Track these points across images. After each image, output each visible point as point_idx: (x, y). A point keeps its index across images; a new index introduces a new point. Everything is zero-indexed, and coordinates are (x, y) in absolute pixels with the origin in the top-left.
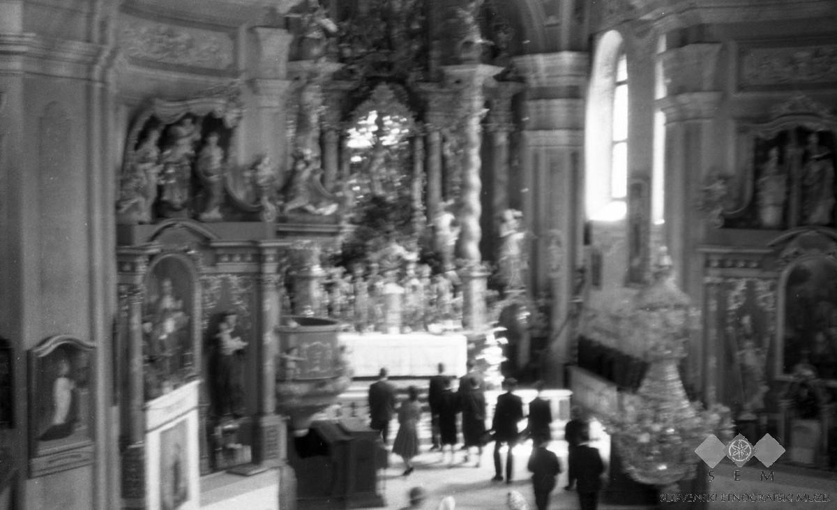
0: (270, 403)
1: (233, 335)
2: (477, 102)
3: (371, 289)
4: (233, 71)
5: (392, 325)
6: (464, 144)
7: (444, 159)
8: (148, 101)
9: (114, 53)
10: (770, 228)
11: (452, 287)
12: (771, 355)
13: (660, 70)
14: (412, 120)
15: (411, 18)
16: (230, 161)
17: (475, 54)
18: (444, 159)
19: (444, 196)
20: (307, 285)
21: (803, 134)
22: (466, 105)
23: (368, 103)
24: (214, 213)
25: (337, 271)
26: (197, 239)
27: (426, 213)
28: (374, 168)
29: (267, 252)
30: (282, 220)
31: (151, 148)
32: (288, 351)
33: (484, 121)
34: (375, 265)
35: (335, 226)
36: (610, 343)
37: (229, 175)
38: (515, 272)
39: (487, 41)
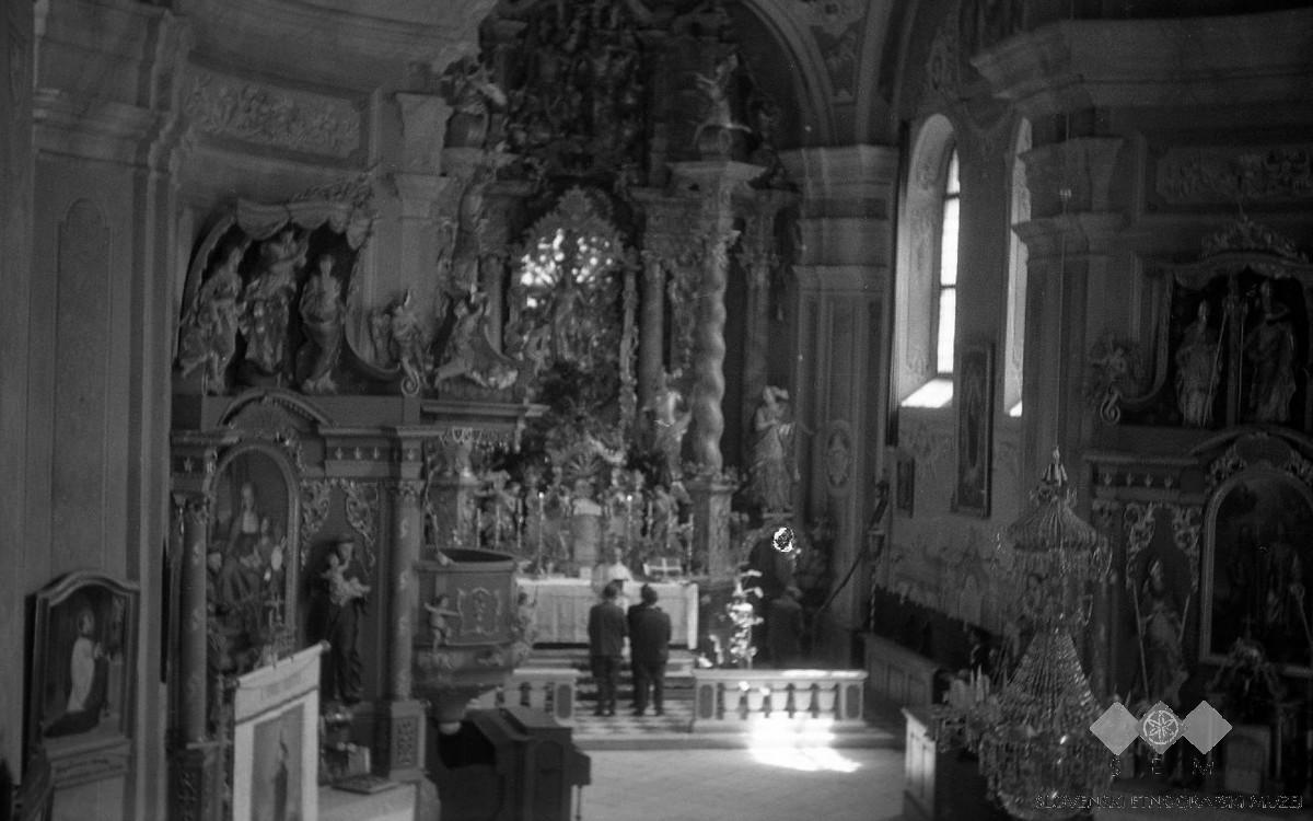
0: (404, 681)
1: (347, 576)
2: (725, 220)
3: (553, 505)
4: (359, 160)
5: (584, 563)
6: (703, 282)
7: (668, 306)
8: (228, 203)
9: (181, 126)
10: (1194, 426)
11: (676, 508)
12: (1194, 623)
13: (1019, 170)
14: (618, 245)
15: (622, 86)
16: (350, 299)
17: (722, 146)
18: (668, 306)
19: (667, 363)
20: (454, 498)
21: (1249, 279)
22: (705, 224)
23: (550, 217)
24: (326, 381)
25: (499, 478)
26: (295, 422)
27: (637, 390)
28: (559, 319)
29: (405, 445)
30: (431, 393)
31: (229, 273)
32: (436, 602)
33: (733, 251)
34: (558, 470)
35: (516, 406)
36: (929, 600)
37: (348, 320)
38: (778, 489)
39: (740, 127)
